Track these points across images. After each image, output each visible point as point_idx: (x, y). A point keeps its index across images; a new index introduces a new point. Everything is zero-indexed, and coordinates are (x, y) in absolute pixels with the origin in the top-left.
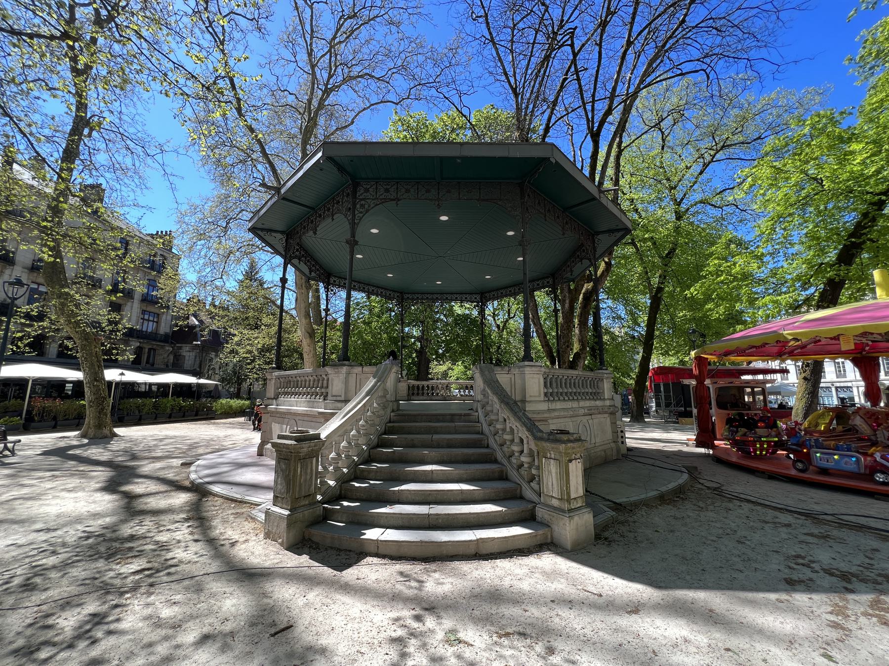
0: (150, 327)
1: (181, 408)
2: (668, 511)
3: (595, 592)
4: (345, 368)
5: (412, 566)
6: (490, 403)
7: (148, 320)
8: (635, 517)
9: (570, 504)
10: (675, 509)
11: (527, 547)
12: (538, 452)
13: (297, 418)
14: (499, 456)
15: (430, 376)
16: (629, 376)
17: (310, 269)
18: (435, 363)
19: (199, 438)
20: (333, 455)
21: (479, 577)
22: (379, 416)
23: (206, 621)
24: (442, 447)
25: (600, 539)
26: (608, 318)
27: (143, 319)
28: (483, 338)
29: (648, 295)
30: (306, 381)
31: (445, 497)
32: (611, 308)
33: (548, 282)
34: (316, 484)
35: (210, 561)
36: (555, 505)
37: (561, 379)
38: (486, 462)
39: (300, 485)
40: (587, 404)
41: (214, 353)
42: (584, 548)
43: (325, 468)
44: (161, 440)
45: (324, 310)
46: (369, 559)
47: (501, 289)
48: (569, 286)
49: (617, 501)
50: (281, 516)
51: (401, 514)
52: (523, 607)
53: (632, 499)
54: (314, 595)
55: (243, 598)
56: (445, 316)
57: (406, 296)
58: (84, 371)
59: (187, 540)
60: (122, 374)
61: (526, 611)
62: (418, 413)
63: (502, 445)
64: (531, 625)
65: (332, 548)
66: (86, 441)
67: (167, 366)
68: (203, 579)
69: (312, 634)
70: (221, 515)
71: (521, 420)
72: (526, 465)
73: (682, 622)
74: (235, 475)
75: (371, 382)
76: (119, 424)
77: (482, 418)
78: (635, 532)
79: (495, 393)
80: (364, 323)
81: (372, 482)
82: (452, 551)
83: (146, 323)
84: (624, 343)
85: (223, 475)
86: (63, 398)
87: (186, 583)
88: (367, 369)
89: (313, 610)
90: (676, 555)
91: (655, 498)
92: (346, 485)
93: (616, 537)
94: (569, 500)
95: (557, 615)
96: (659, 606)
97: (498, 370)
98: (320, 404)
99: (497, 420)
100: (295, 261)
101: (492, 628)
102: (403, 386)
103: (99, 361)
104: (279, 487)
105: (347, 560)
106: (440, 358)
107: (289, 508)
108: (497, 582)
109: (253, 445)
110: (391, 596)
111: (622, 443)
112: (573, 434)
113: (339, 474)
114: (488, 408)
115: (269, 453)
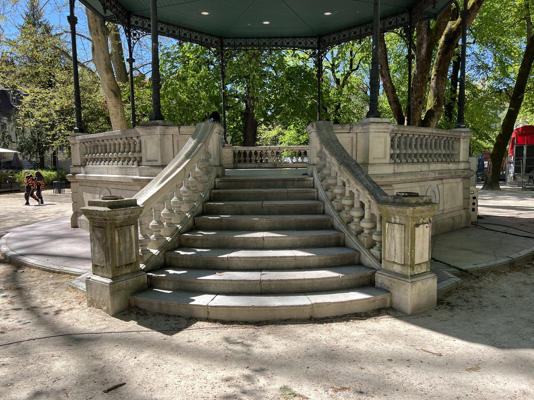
2: (517, 277)
3: (435, 352)
5: (244, 330)
6: (328, 165)
8: (481, 284)
9: (413, 270)
10: (525, 275)
11: (365, 311)
12: (381, 218)
13: (110, 187)
14: (336, 222)
15: (258, 143)
16: (488, 138)
17: (103, 5)
18: (264, 127)
19: (6, 211)
20: (153, 223)
21: (314, 339)
22: (202, 182)
23: (37, 381)
24: (274, 214)
25: (442, 304)
26: (472, 67)
28: (319, 97)
29: (524, 38)
30: (115, 144)
31: (278, 264)
32: (477, 55)
33: (403, 19)
34: (137, 252)
35: (34, 328)
36: (397, 271)
37: (411, 138)
39: (120, 254)
40: (439, 167)
41: (5, 118)
42: (425, 312)
43: (145, 236)
45: (128, 60)
46: (199, 324)
47: (345, 29)
48: (429, 24)
50: (103, 285)
51: (231, 280)
52: (359, 365)
53: (479, 266)
54: (146, 357)
55: (72, 360)
56: (274, 68)
57: (226, 42)
59: (8, 309)
61: (362, 369)
62: (246, 178)
63: (339, 211)
64: (368, 381)
65: (160, 314)
68: (29, 344)
69: (145, 390)
70: (40, 286)
71: (362, 183)
72: (366, 231)
73: (522, 378)
74: (50, 247)
75: (191, 143)
77: (318, 183)
78: (481, 297)
79: (334, 154)
80: (179, 78)
81: (198, 250)
82: (285, 315)
84: (486, 98)
85: (36, 247)
87: (12, 347)
88: (184, 129)
89: (144, 370)
90: (522, 319)
91: (504, 265)
92: (170, 253)
93: (459, 302)
94: (413, 266)
95: (395, 372)
96: (500, 364)
97: (337, 128)
98: (134, 171)
99: (335, 185)
101: (327, 384)
102: (228, 153)
104: (97, 256)
105: (177, 325)
106: (269, 121)
107: (110, 276)
108: (333, 343)
109: (65, 218)
110: (224, 356)
111: (473, 210)
112: (423, 196)
113: (162, 242)
114: (326, 172)
115: (84, 225)
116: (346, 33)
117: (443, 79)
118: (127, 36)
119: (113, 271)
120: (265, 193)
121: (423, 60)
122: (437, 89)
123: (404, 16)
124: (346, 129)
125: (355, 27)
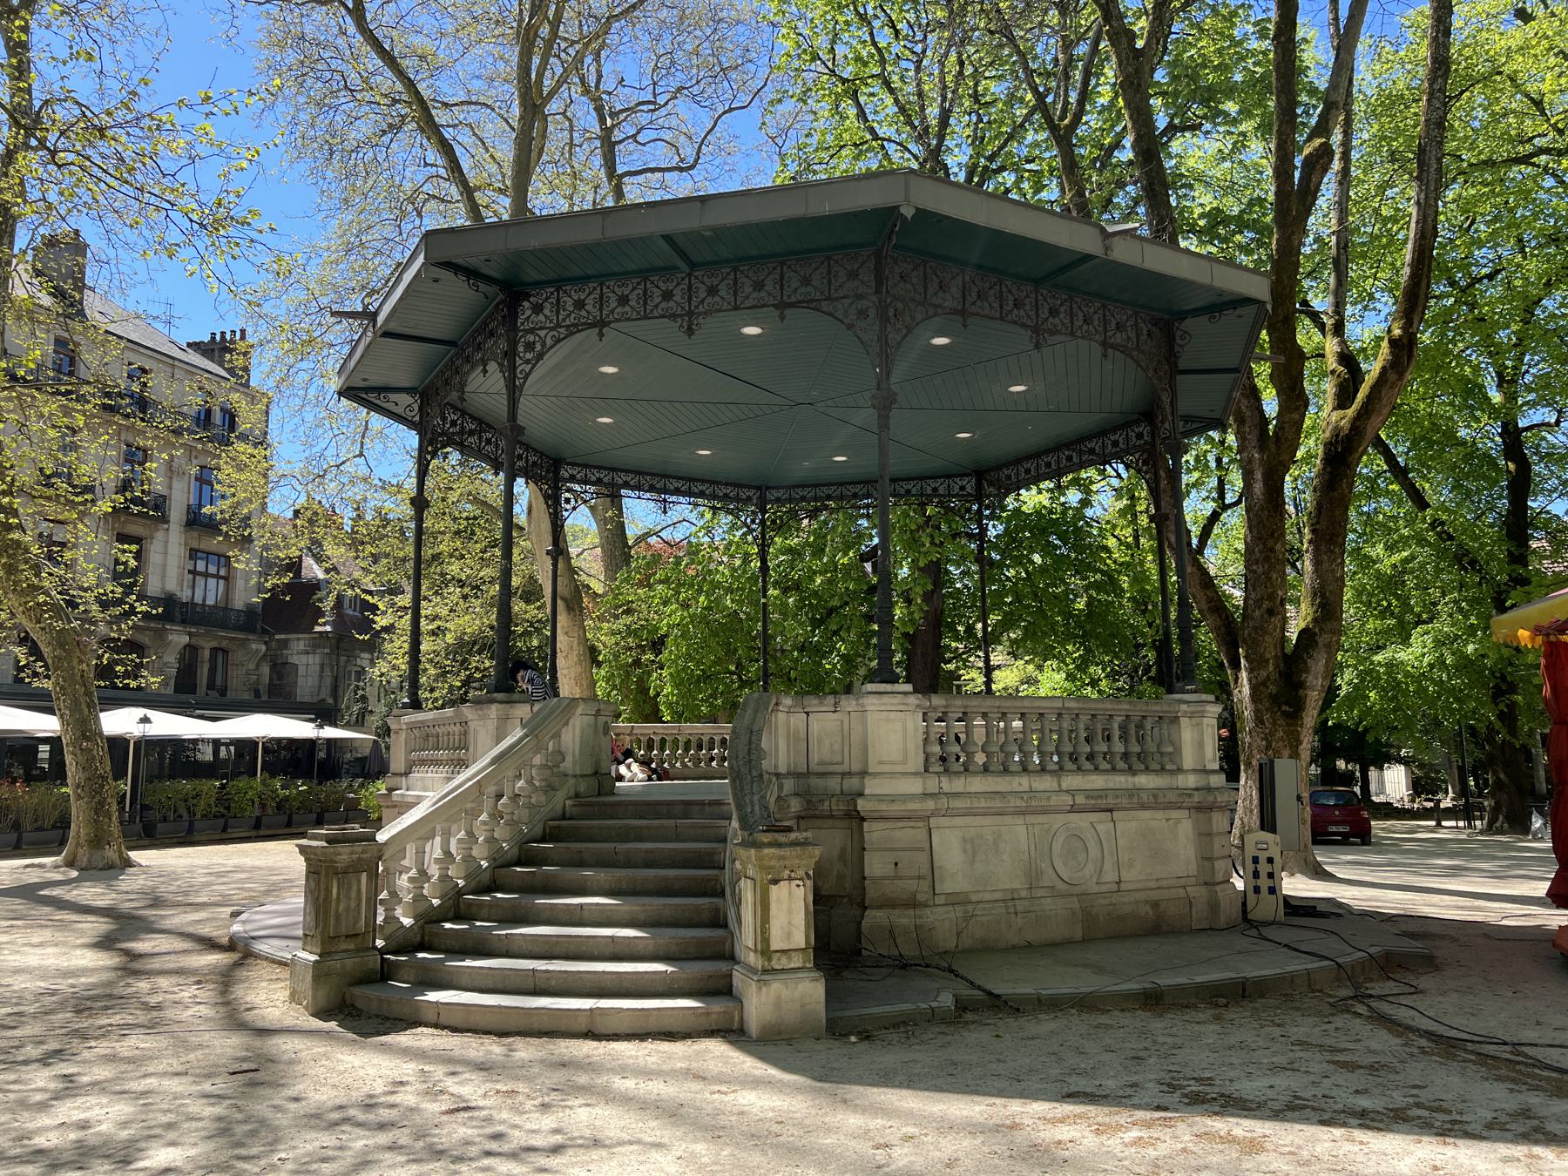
0: (209, 593)
1: (281, 805)
4: (494, 707)
7: (206, 575)
27: (193, 572)
38: (704, 894)
39: (338, 916)
41: (366, 655)
44: (219, 875)
47: (1028, 458)
49: (996, 992)
50: (305, 963)
58: (62, 717)
60: (145, 720)
66: (74, 874)
67: (257, 694)
76: (146, 842)
83: (200, 581)
86: (29, 779)
92: (434, 926)
103: (88, 694)
113: (422, 907)
116: (1095, 445)
117: (1332, 552)
118: (549, 507)
119: (323, 944)
120: (635, 828)
121: (1262, 509)
122: (1319, 577)
123: (1141, 429)
124: (828, 705)
125: (1047, 452)
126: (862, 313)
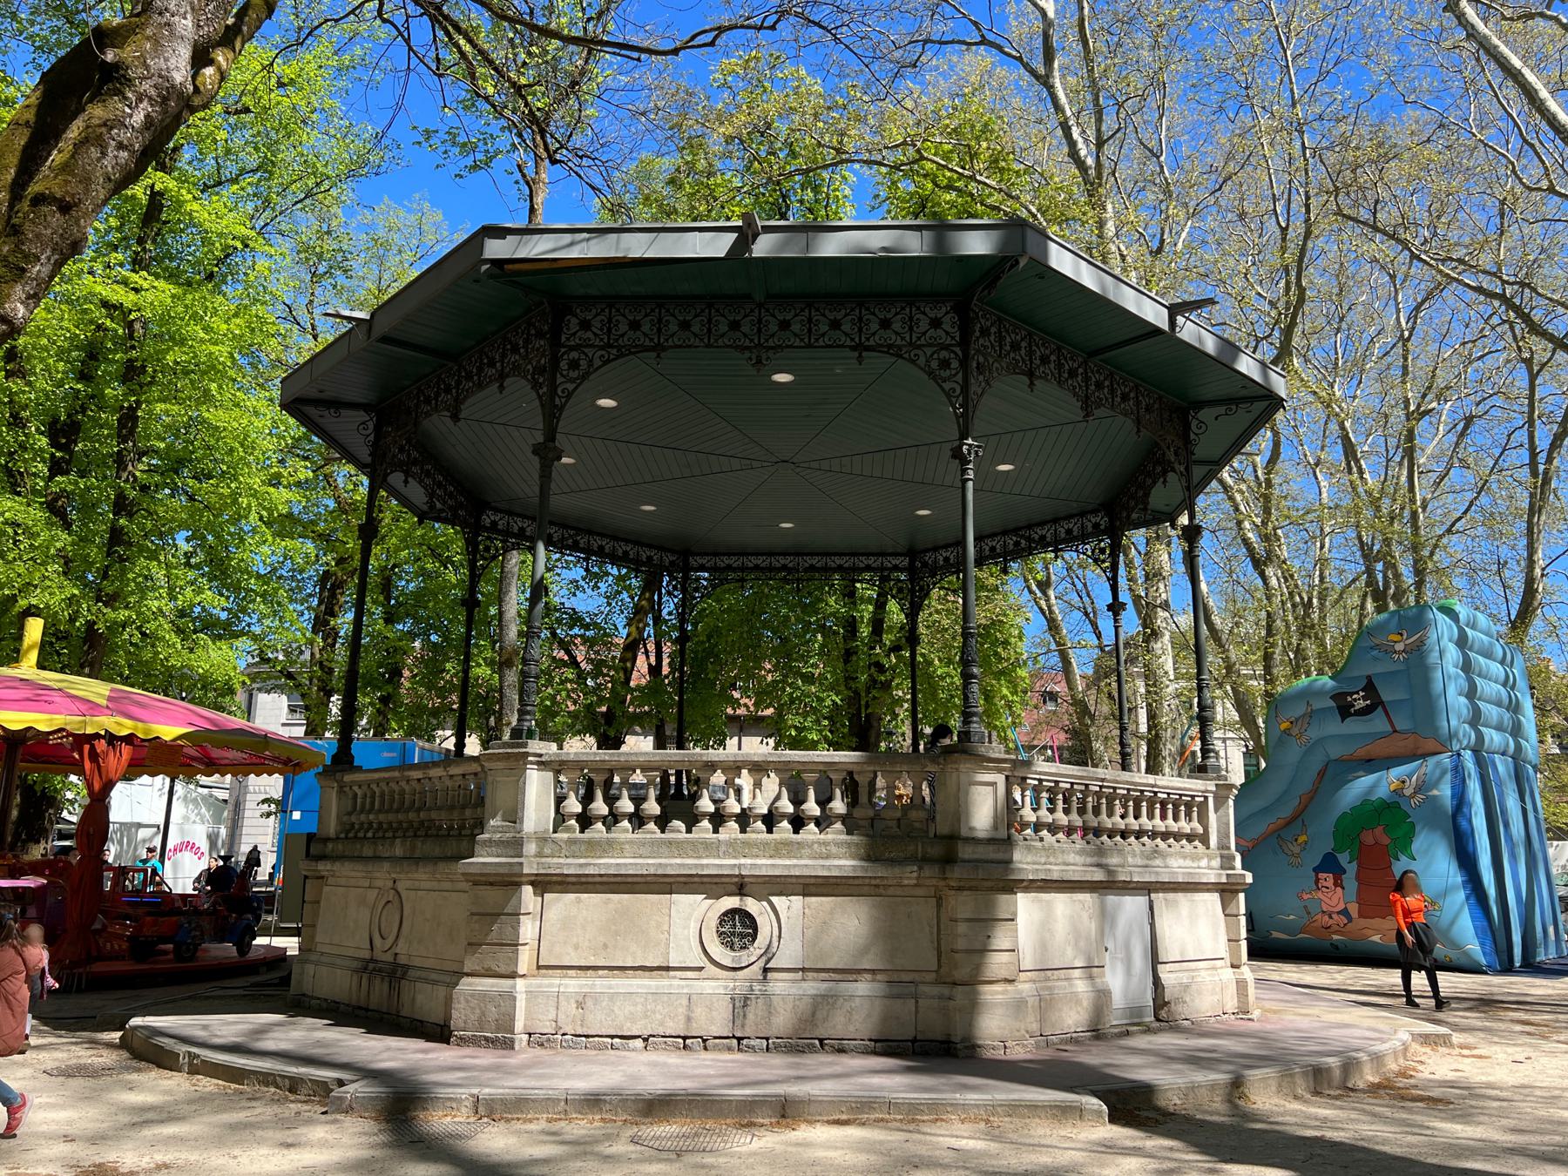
100: (396, 479)
126: (945, 364)
